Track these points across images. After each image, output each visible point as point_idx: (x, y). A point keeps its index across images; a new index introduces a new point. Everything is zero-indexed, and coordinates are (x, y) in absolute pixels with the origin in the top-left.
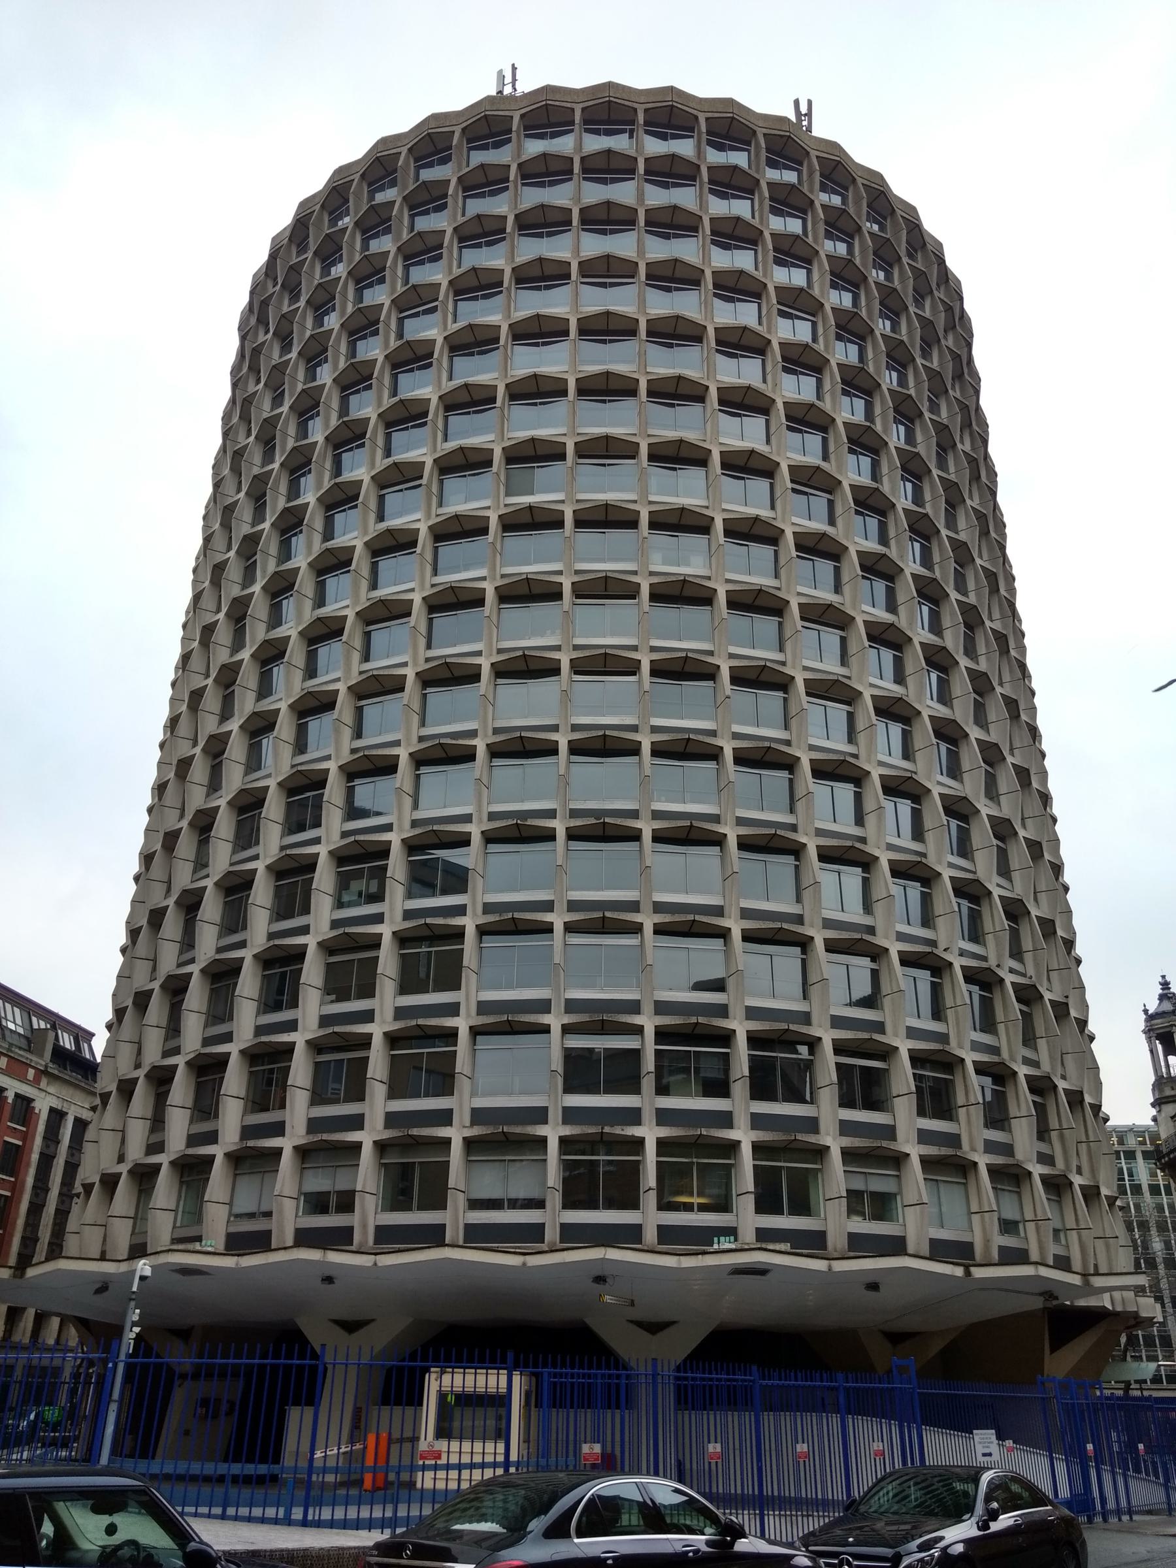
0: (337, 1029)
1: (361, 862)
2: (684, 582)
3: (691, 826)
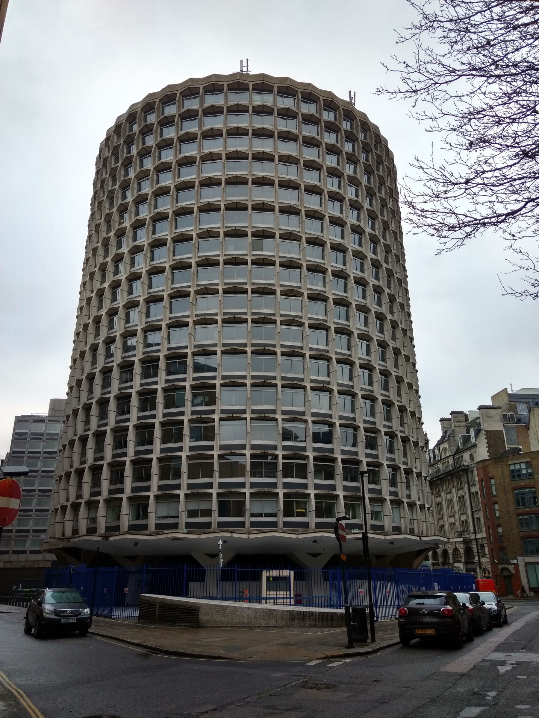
0: (146, 387)
1: (150, 366)
2: (264, 203)
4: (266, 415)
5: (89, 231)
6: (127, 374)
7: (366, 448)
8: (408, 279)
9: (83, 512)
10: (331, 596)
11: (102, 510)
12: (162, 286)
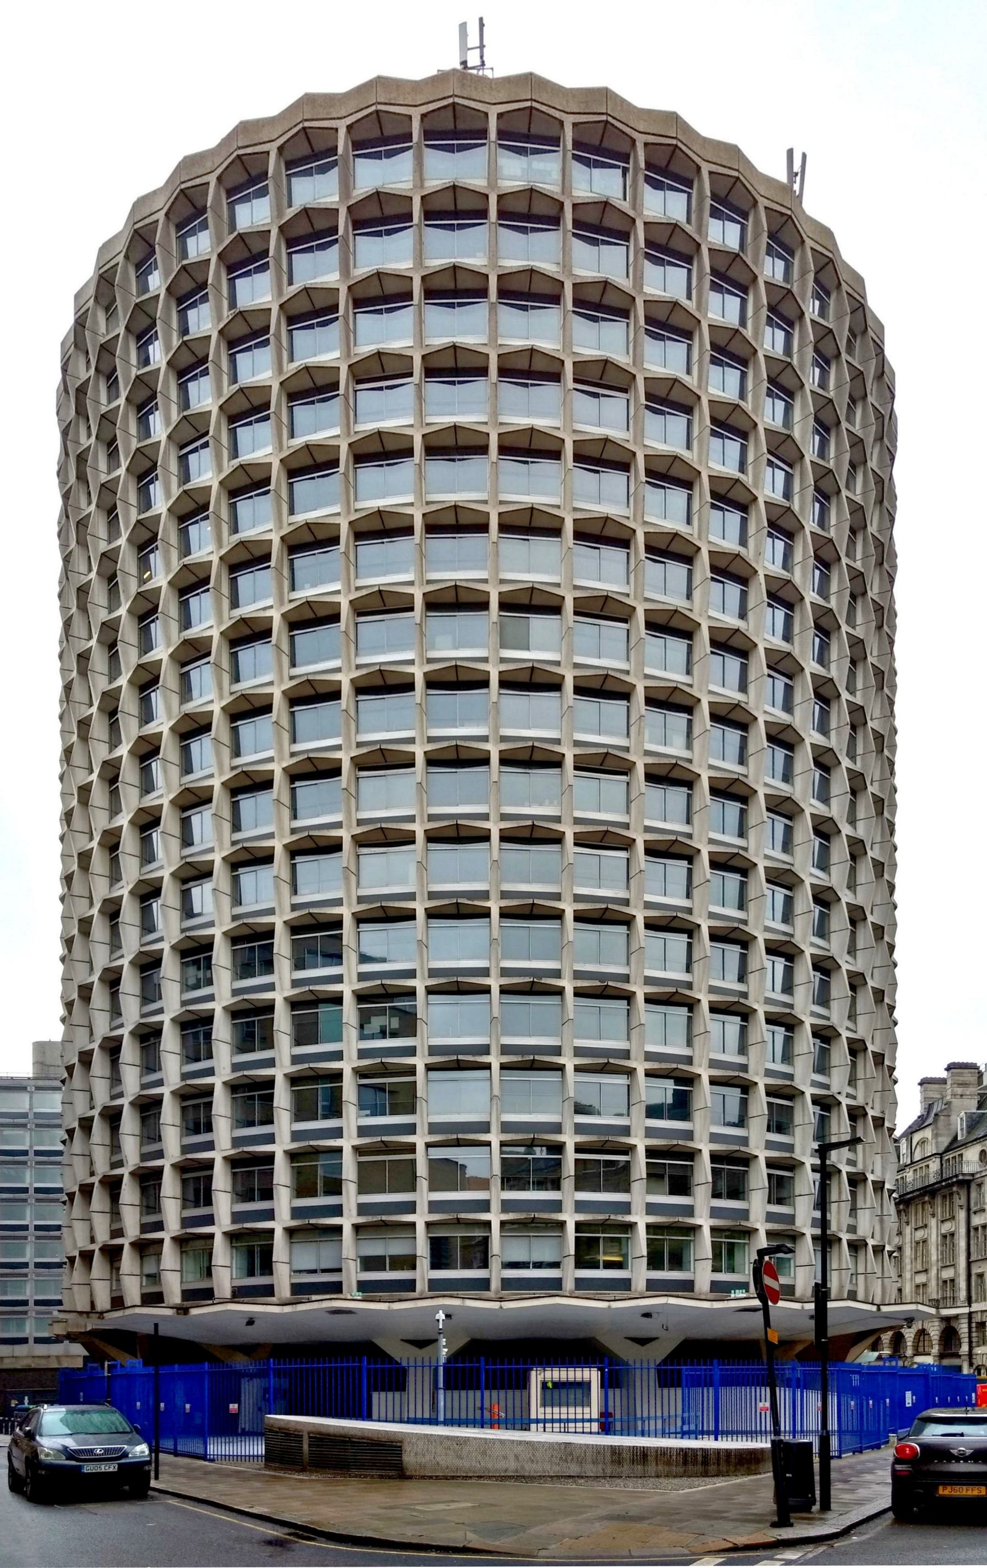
3: (533, 825)
4: (537, 1057)
5: (64, 608)
6: (199, 969)
7: (769, 1130)
8: (897, 738)
9: (128, 1261)
10: (686, 1415)
11: (169, 1257)
12: (265, 746)
